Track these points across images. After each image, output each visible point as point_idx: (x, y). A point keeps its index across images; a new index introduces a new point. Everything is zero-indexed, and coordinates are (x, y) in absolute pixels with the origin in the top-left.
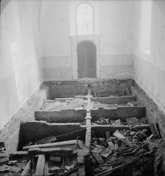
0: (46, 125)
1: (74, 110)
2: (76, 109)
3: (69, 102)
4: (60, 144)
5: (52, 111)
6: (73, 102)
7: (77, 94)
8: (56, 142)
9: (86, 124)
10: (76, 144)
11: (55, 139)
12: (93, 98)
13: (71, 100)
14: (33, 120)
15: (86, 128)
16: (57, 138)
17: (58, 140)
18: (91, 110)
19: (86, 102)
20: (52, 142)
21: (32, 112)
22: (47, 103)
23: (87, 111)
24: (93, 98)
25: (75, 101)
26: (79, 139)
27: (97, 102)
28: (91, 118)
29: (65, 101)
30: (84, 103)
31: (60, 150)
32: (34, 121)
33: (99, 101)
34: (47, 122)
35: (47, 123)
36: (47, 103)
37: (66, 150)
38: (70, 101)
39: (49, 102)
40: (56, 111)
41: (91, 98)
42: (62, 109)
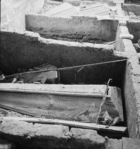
0: (38, 41)
1: (96, 19)
2: (100, 18)
3: (84, 7)
4: (64, 90)
5: (55, 16)
6: (91, 7)
7: (52, 64)
8: (56, 81)
9: (126, 50)
10: (104, 99)
11: (54, 74)
12: (124, 4)
13: (88, 4)
14: (20, 30)
15: (126, 58)
16: (60, 73)
17: (63, 79)
18: (127, 22)
19: (113, 8)
20: (48, 82)
21: (20, 14)
22: (50, 6)
23: (120, 22)
24: (124, 4)
25: (94, 5)
26: (111, 84)
27: (130, 13)
28: (132, 36)
29: (78, 5)
30: (111, 10)
31: (62, 139)
32: (22, 33)
33: (133, 12)
34: (42, 35)
35: (40, 39)
36: (50, 6)
37: (83, 137)
38: (86, 6)
39: (53, 4)
40: (62, 17)
41: (122, 4)
42: (73, 15)
